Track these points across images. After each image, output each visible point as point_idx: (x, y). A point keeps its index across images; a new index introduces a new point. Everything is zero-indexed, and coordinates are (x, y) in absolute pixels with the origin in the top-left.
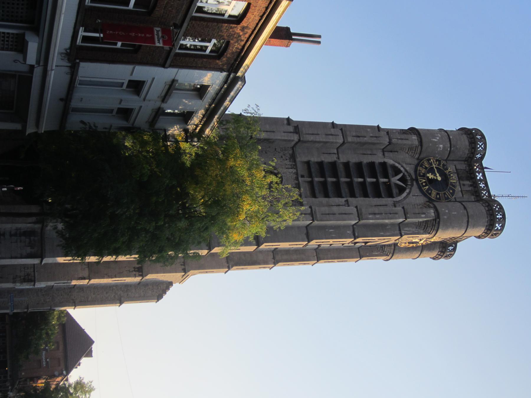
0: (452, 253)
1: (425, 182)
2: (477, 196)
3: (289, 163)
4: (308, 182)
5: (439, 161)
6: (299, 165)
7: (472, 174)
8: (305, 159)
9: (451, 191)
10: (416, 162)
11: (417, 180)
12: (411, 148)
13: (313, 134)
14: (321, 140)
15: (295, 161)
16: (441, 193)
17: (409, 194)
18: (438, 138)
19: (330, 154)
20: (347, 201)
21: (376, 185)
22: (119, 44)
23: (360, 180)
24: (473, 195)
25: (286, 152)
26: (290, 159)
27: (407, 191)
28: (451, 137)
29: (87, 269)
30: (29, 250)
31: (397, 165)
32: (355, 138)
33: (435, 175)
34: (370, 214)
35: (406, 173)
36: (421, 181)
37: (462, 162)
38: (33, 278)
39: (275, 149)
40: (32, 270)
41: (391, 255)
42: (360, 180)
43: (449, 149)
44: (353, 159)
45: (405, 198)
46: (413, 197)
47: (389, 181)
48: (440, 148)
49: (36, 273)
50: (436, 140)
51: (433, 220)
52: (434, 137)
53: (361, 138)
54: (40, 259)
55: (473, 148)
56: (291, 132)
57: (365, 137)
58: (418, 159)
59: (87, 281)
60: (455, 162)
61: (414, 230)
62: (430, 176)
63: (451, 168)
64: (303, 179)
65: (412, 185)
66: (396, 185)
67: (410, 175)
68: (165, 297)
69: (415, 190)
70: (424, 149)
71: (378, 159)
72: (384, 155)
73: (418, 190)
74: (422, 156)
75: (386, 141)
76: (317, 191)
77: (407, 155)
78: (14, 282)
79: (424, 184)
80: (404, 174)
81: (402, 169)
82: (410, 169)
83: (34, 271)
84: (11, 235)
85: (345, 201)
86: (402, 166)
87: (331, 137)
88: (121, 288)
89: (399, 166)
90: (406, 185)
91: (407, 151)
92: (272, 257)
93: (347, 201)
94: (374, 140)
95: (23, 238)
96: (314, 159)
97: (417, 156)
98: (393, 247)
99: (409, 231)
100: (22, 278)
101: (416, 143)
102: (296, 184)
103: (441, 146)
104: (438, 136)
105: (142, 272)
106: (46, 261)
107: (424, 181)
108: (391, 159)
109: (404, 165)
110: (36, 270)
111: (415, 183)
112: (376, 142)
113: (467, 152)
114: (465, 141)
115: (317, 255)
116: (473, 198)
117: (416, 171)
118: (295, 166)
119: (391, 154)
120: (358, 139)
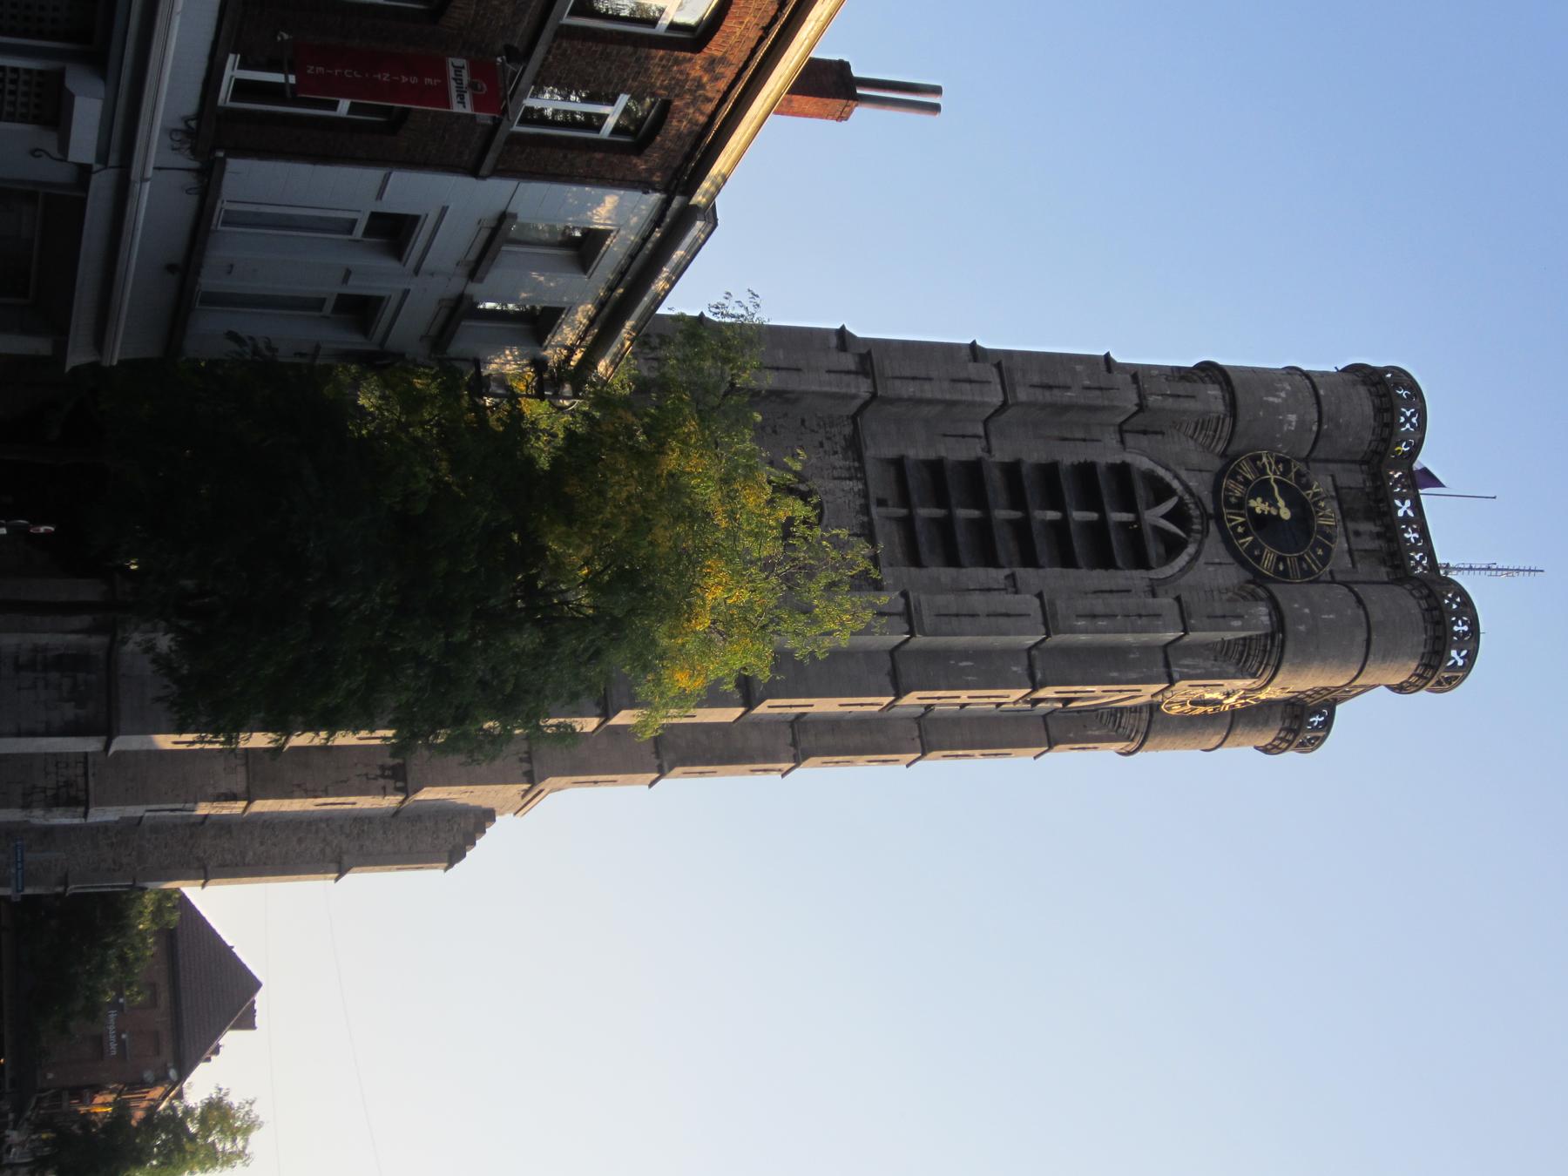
0: (1321, 734)
1: (1242, 524)
2: (1396, 567)
3: (842, 463)
4: (899, 520)
5: (1286, 462)
6: (872, 470)
7: (1381, 501)
8: (891, 452)
9: (1320, 552)
10: (1217, 464)
11: (1219, 518)
12: (1202, 424)
13: (914, 378)
14: (939, 396)
15: (860, 457)
16: (1291, 557)
17: (1194, 558)
18: (1283, 394)
19: (963, 436)
20: (1012, 577)
21: (1098, 531)
22: (344, 106)
23: (1052, 515)
24: (1383, 562)
25: (835, 430)
26: (845, 450)
27: (1191, 549)
28: (1322, 392)
29: (242, 770)
30: (69, 711)
31: (1161, 472)
32: (1038, 392)
33: (1274, 504)
34: (1079, 616)
35: (1187, 497)
36: (1231, 521)
37: (1353, 466)
38: (81, 795)
39: (803, 421)
40: (80, 771)
41: (1139, 739)
42: (1052, 515)
43: (1315, 428)
44: (1033, 453)
45: (1183, 570)
46: (1209, 568)
47: (1138, 520)
48: (1290, 423)
49: (91, 778)
50: (1276, 400)
51: (1266, 635)
52: (1273, 391)
53: (1056, 392)
54: (104, 738)
55: (1386, 425)
56: (848, 372)
57: (1067, 388)
58: (1223, 455)
59: (243, 804)
60: (1331, 466)
61: (1209, 664)
62: (1259, 505)
63: (1320, 484)
64: (882, 510)
65: (1205, 532)
66: (1158, 530)
67: (1199, 502)
68: (471, 854)
69: (1214, 547)
70: (1240, 427)
71: (1106, 453)
72: (1122, 442)
73: (1222, 548)
74: (1234, 448)
75: (1130, 400)
76: (924, 549)
77: (1191, 443)
78: (27, 806)
79: (1240, 530)
80: (1181, 499)
81: (1175, 484)
82: (1200, 484)
83: (86, 774)
84: (18, 667)
85: (1007, 577)
86: (1177, 477)
87: (967, 386)
88: (341, 827)
89: (1168, 477)
90: (1188, 531)
91: (1190, 432)
92: (789, 740)
93: (1012, 577)
94: (1095, 398)
95: (54, 676)
96: (917, 452)
97: (1220, 447)
98: (1145, 715)
99: (1195, 667)
100: (50, 793)
101: (1219, 407)
102: (862, 525)
103: (1293, 418)
104: (1283, 389)
105: (404, 779)
106: (121, 743)
107: (1241, 519)
108: (1143, 453)
109: (1184, 474)
110: (90, 772)
111: (1213, 527)
112: (1099, 402)
113: (1368, 436)
114: (1362, 404)
115: (920, 736)
116: (1383, 573)
117: (1216, 489)
118: (859, 473)
119: (1144, 441)
120: (1047, 393)
